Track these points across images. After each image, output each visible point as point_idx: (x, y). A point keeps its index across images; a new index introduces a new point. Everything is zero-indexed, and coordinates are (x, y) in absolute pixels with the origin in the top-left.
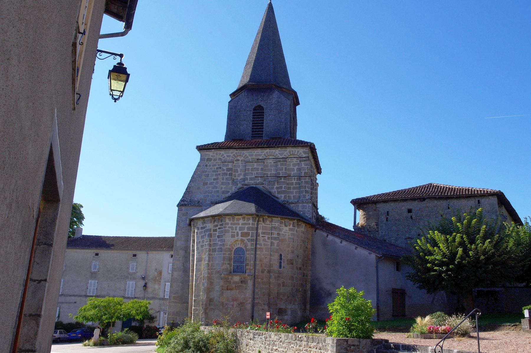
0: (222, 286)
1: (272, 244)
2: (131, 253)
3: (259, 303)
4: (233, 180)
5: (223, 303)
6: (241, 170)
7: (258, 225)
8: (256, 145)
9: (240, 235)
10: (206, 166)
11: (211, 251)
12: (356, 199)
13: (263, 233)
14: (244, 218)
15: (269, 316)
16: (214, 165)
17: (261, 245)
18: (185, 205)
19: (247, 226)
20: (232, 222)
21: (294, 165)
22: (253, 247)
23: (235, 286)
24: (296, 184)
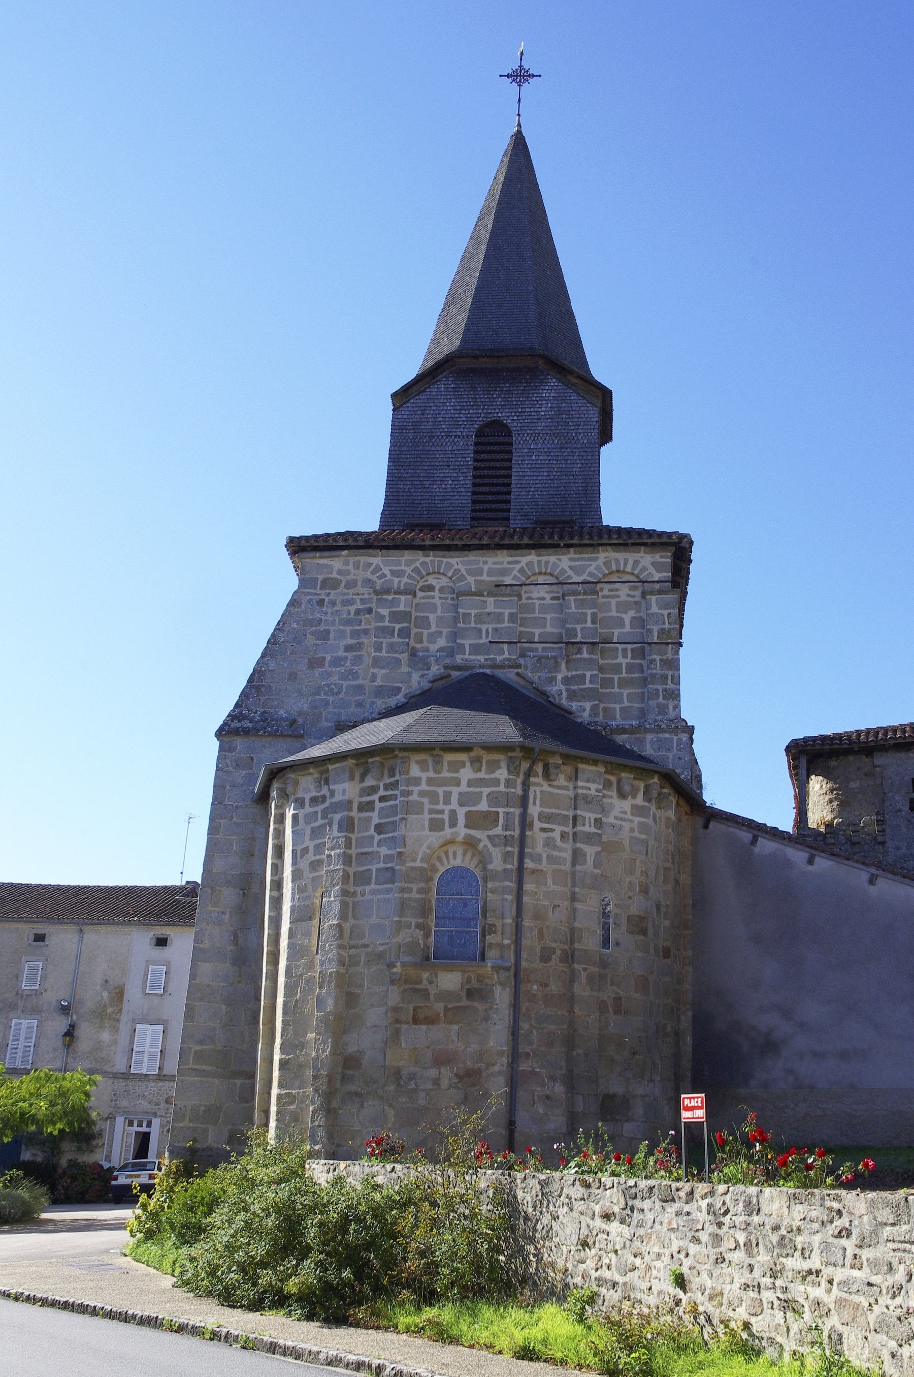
0: (396, 1009)
1: (577, 857)
2: (27, 930)
3: (532, 1072)
4: (413, 653)
5: (397, 1074)
6: (440, 619)
7: (526, 786)
8: (492, 537)
9: (461, 821)
10: (321, 602)
11: (354, 880)
12: (806, 739)
13: (543, 817)
14: (476, 763)
15: (701, 1113)
16: (350, 602)
17: (537, 859)
18: (246, 732)
19: (486, 791)
20: (431, 774)
21: (623, 607)
22: (512, 866)
23: (446, 1009)
24: (630, 668)
